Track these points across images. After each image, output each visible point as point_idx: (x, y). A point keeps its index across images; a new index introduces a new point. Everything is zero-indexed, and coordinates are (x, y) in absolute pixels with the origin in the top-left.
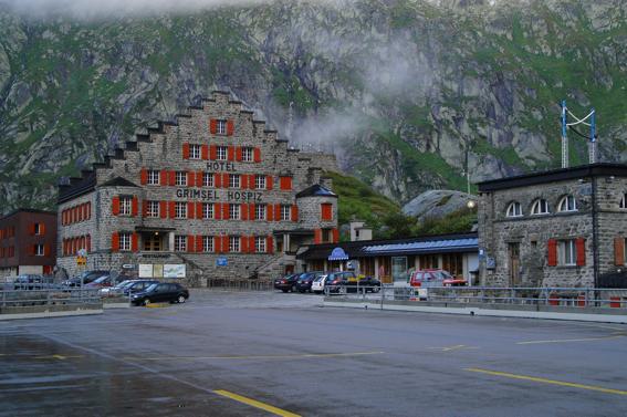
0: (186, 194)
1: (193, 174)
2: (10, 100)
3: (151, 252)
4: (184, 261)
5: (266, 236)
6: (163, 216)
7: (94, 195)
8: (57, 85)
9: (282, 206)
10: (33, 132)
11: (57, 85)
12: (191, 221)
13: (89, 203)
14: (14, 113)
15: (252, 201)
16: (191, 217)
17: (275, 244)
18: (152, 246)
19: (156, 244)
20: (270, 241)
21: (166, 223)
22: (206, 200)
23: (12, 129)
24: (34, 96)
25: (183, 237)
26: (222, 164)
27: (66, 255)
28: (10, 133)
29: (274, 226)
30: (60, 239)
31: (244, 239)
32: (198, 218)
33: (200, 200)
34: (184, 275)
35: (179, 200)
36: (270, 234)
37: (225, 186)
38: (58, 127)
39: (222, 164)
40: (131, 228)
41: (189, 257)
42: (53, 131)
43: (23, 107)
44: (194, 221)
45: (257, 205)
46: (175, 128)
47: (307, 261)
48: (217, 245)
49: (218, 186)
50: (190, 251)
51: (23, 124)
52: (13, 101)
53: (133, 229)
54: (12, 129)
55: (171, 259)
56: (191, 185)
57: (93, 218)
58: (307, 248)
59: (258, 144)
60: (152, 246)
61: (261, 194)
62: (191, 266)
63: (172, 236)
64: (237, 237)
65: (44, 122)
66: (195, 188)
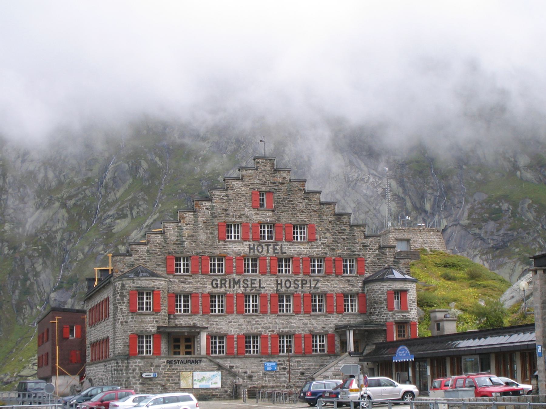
0: (223, 284)
1: (231, 259)
2: (107, 184)
3: (182, 356)
4: (220, 367)
5: (327, 334)
6: (195, 313)
7: (111, 288)
8: (159, 163)
9: (345, 295)
10: (132, 218)
11: (159, 163)
12: (230, 317)
13: (108, 298)
14: (111, 198)
15: (306, 289)
16: (230, 312)
17: (337, 343)
18: (182, 349)
19: (188, 347)
20: (331, 339)
21: (198, 320)
22: (248, 290)
23: (109, 217)
24: (135, 178)
25: (222, 337)
26: (268, 246)
27: (94, 361)
28: (108, 221)
29: (335, 320)
30: (88, 342)
31: (298, 337)
32: (239, 313)
33: (241, 290)
34: (219, 385)
35: (215, 290)
36: (331, 331)
37: (273, 274)
38: (161, 212)
39: (268, 246)
40: (152, 328)
41: (227, 363)
42: (155, 217)
43: (122, 190)
44: (234, 317)
45: (313, 295)
46: (208, 204)
47: (374, 362)
48: (265, 347)
49: (263, 273)
50: (230, 355)
51: (122, 210)
52: (110, 184)
53: (154, 330)
54: (109, 217)
55: (203, 364)
56: (229, 273)
57: (111, 317)
58: (374, 347)
59: (314, 220)
60: (182, 349)
61: (318, 281)
62: (228, 372)
63: (203, 338)
64: (289, 336)
65: (145, 206)
66: (234, 276)
